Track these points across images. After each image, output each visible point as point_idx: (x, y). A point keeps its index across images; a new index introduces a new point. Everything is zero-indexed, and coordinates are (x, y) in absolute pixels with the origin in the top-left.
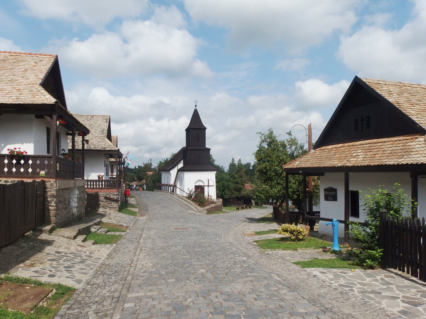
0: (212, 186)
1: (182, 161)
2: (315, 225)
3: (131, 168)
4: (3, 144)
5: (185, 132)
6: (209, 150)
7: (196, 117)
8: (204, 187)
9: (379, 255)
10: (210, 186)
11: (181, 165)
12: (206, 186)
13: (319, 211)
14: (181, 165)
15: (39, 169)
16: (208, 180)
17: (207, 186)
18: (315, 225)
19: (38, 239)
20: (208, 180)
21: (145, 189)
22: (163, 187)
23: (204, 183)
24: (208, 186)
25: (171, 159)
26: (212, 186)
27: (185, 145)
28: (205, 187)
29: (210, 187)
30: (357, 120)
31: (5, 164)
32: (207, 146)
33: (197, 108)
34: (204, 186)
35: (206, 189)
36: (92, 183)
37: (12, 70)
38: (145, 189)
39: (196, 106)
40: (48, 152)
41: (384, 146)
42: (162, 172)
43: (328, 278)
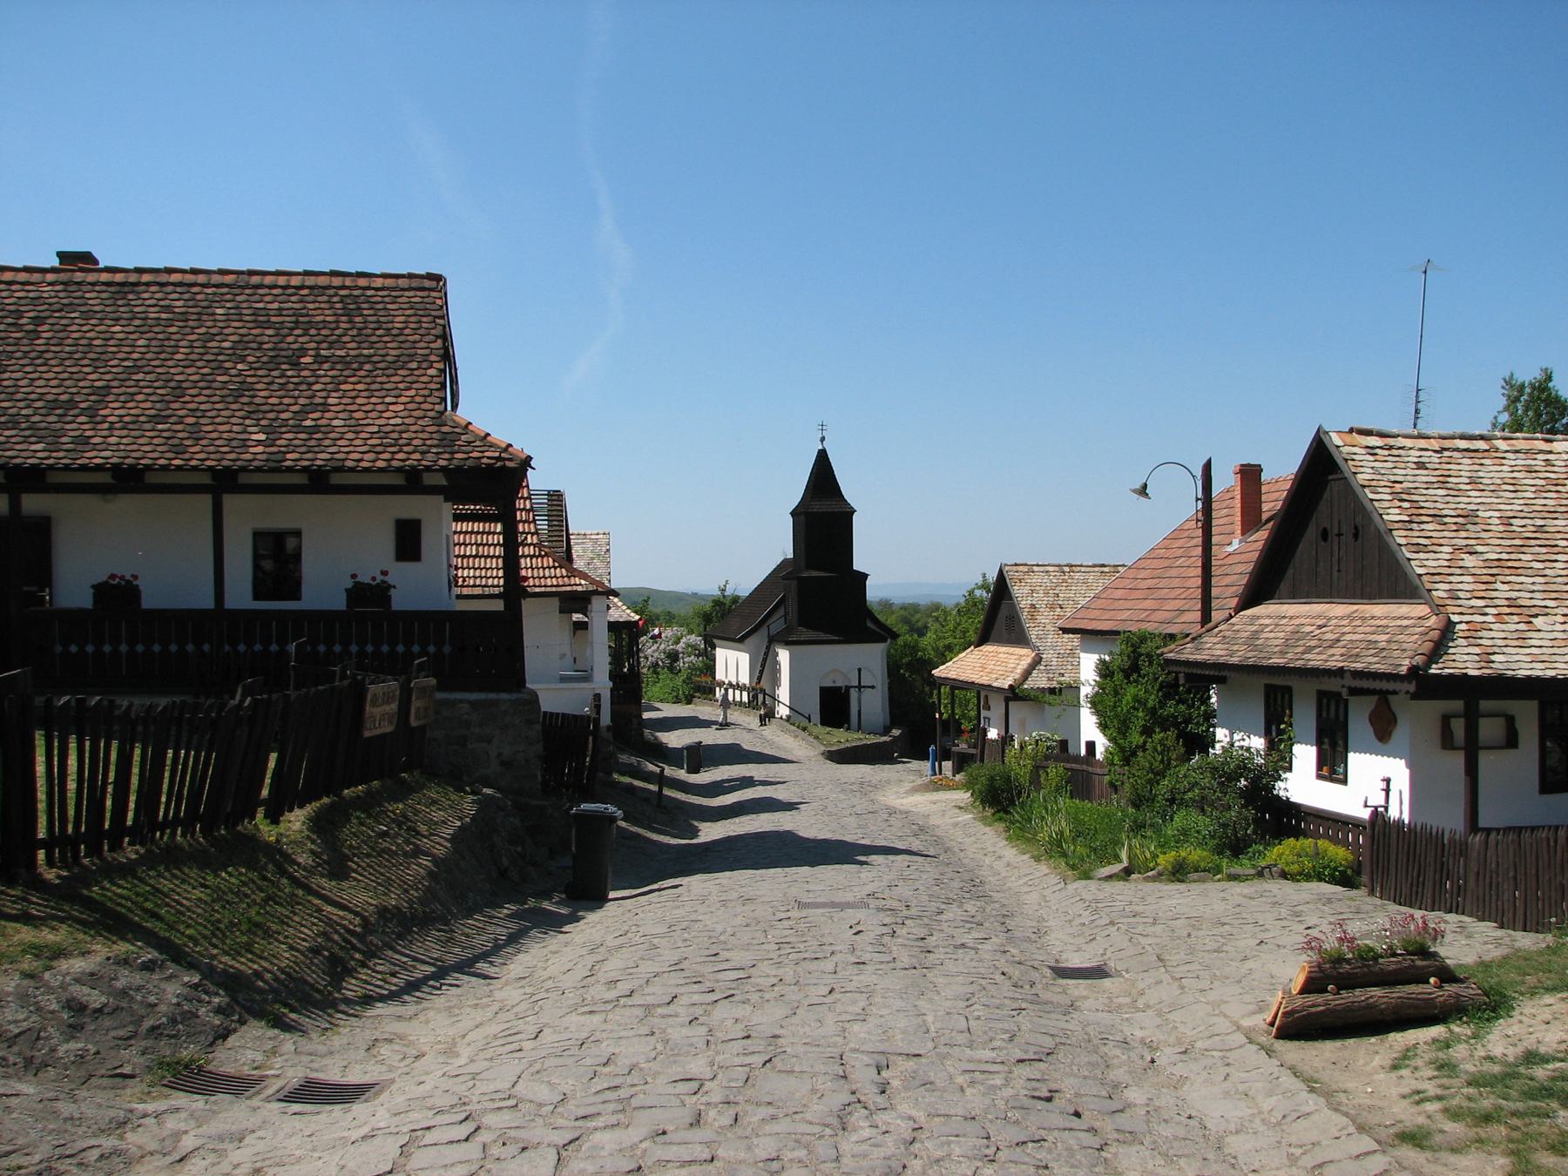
0: (869, 687)
1: (781, 612)
3: (1368, 755)
6: (863, 577)
7: (823, 478)
9: (59, 877)
10: (864, 687)
11: (777, 625)
13: (1545, 797)
15: (81, 612)
16: (860, 670)
20: (860, 670)
21: (783, 711)
23: (850, 680)
24: (860, 687)
26: (869, 687)
28: (852, 690)
29: (867, 693)
31: (356, 644)
34: (848, 688)
35: (854, 694)
38: (783, 711)
39: (823, 439)
40: (986, 697)
41: (1481, 474)
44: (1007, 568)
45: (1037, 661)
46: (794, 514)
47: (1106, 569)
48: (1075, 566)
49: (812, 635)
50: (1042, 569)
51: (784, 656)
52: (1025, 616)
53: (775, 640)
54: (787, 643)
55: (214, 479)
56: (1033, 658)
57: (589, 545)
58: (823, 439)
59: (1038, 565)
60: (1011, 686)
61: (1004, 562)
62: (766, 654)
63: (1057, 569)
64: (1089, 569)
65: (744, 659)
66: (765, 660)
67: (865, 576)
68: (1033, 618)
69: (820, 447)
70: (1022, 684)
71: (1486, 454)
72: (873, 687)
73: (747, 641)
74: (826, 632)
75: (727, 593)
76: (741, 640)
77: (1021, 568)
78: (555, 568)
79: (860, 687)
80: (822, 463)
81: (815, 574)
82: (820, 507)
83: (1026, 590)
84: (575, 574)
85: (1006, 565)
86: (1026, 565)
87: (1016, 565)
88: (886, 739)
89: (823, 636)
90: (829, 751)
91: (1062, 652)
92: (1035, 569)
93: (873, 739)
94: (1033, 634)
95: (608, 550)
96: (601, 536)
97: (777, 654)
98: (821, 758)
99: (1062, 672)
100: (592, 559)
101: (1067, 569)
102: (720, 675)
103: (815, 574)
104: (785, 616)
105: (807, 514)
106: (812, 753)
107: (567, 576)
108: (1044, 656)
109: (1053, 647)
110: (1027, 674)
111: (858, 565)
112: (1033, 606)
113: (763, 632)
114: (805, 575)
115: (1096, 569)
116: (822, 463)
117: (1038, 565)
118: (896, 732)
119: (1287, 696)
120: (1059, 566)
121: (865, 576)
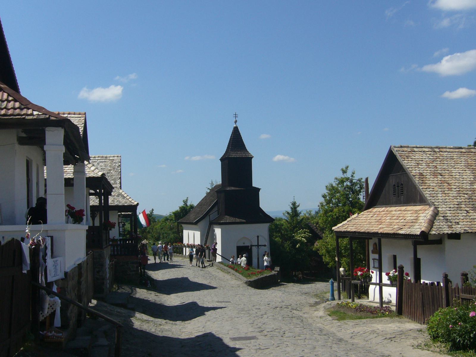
0: (263, 246)
1: (216, 209)
2: (111, 195)
4: (443, 285)
5: (220, 163)
8: (251, 248)
10: (261, 246)
12: (254, 246)
14: (214, 215)
16: (258, 237)
17: (256, 246)
18: (111, 195)
19: (136, 298)
20: (258, 237)
22: (184, 249)
25: (60, 127)
26: (263, 246)
27: (218, 180)
30: (394, 185)
32: (255, 184)
33: (238, 125)
34: (252, 246)
36: (116, 248)
37: (202, 208)
39: (236, 122)
42: (183, 225)
43: (376, 333)
44: (396, 149)
45: (436, 214)
46: (222, 160)
47: (463, 150)
48: (442, 148)
49: (232, 219)
50: (420, 149)
51: (218, 231)
52: (417, 180)
53: (213, 223)
54: (219, 224)
55: (165, 256)
56: (433, 211)
57: (109, 163)
58: (236, 122)
59: (417, 147)
60: (422, 232)
61: (393, 145)
62: (208, 233)
63: (430, 150)
64: (452, 150)
65: (198, 234)
66: (208, 233)
67: (258, 190)
68: (423, 183)
69: (235, 126)
70: (430, 231)
71: (465, 153)
72: (265, 246)
73: (199, 224)
74: (239, 218)
75: (189, 204)
76: (196, 223)
77: (405, 149)
78: (9, 101)
79: (258, 246)
80: (236, 133)
81: (233, 188)
82: (233, 155)
83: (413, 163)
84: (29, 106)
85: (395, 147)
86: (408, 147)
87: (401, 147)
88: (273, 273)
89: (238, 220)
90: (250, 281)
91: (452, 206)
92: (415, 149)
93: (267, 274)
94: (427, 194)
95: (120, 166)
96: (116, 158)
97: (214, 231)
98: (245, 285)
99: (457, 221)
100: (110, 170)
101: (437, 150)
102: (185, 242)
103: (233, 188)
104: (218, 211)
105: (229, 159)
106: (239, 283)
107: (19, 108)
108: (440, 209)
109: (445, 202)
110: (432, 223)
111: (255, 184)
112: (421, 174)
113: (207, 219)
114: (228, 189)
115: (457, 150)
116: (236, 133)
117: (417, 147)
118: (277, 269)
119: (215, 258)
120: (431, 148)
121: (258, 190)
